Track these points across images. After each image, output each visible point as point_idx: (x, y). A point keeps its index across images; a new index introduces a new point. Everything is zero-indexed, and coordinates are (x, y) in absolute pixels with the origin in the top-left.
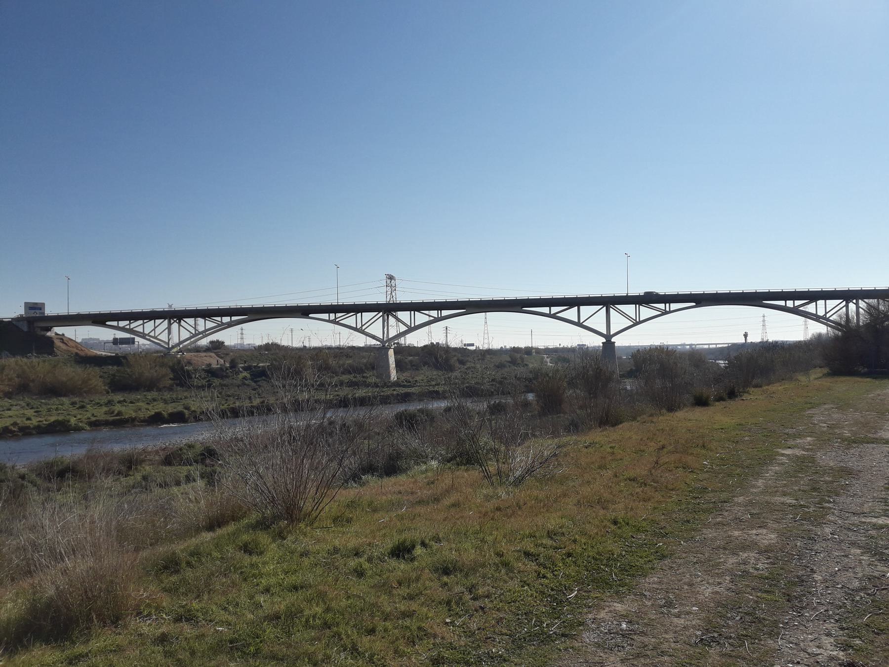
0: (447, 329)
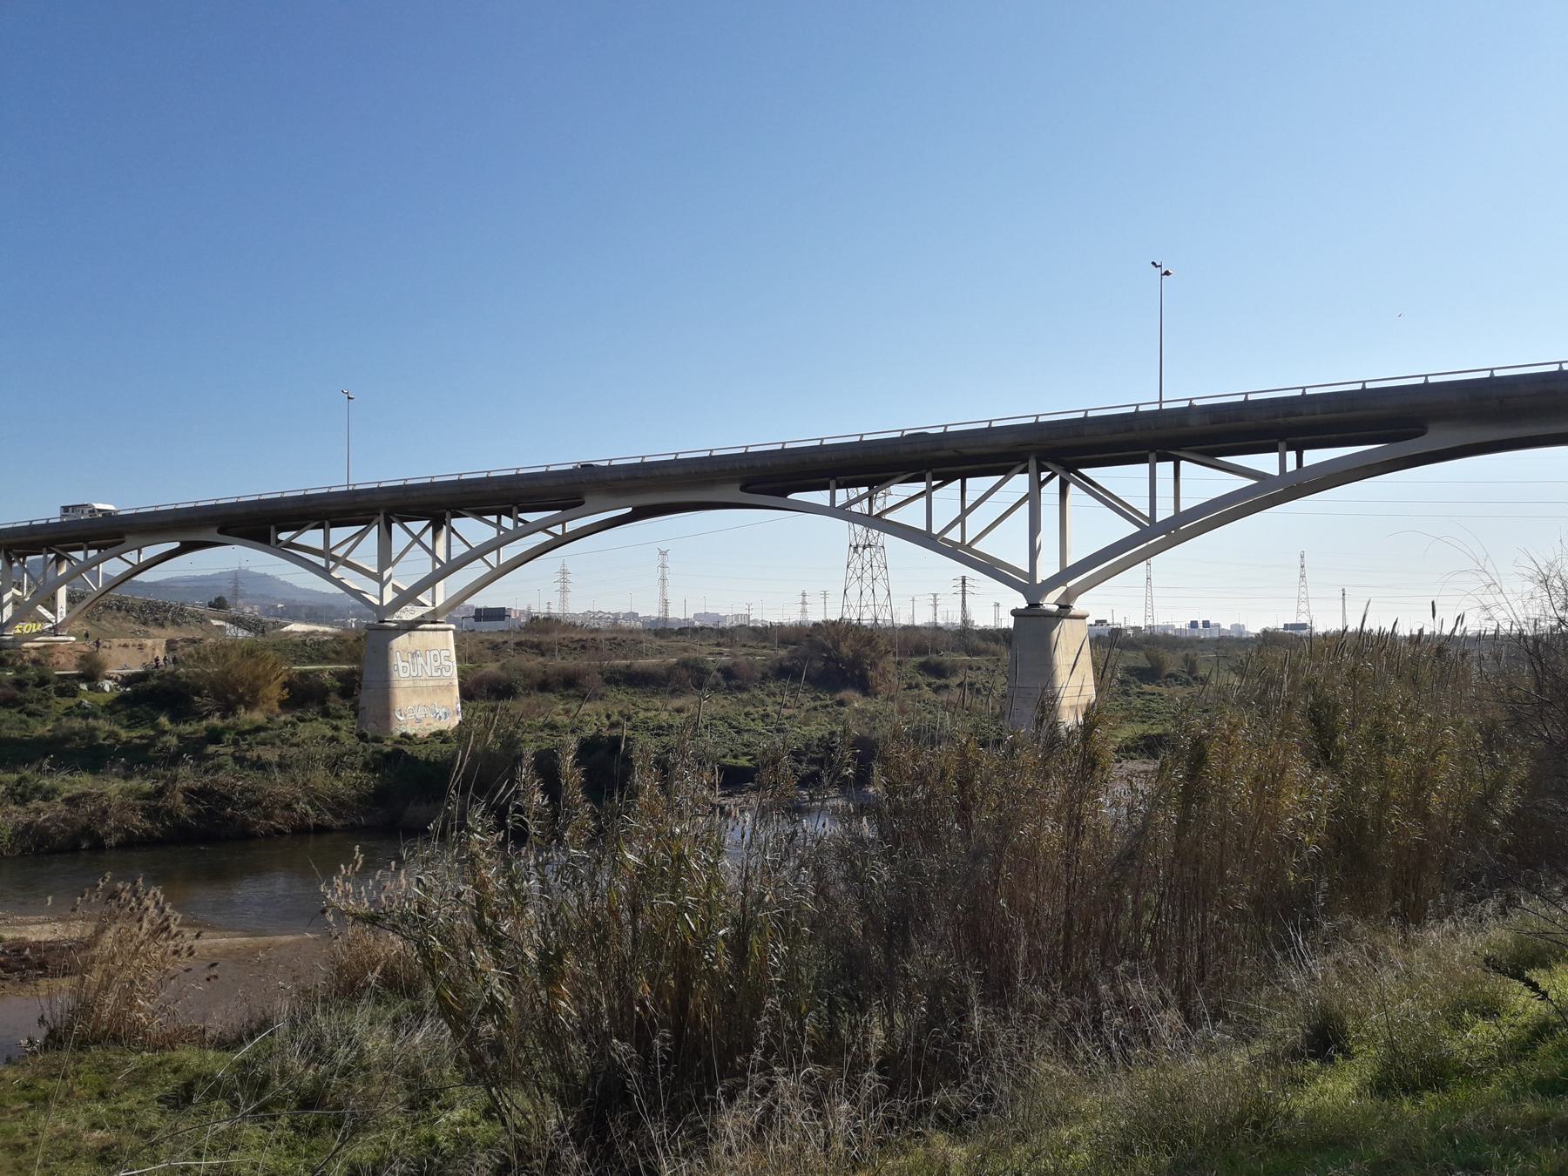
0: (964, 582)
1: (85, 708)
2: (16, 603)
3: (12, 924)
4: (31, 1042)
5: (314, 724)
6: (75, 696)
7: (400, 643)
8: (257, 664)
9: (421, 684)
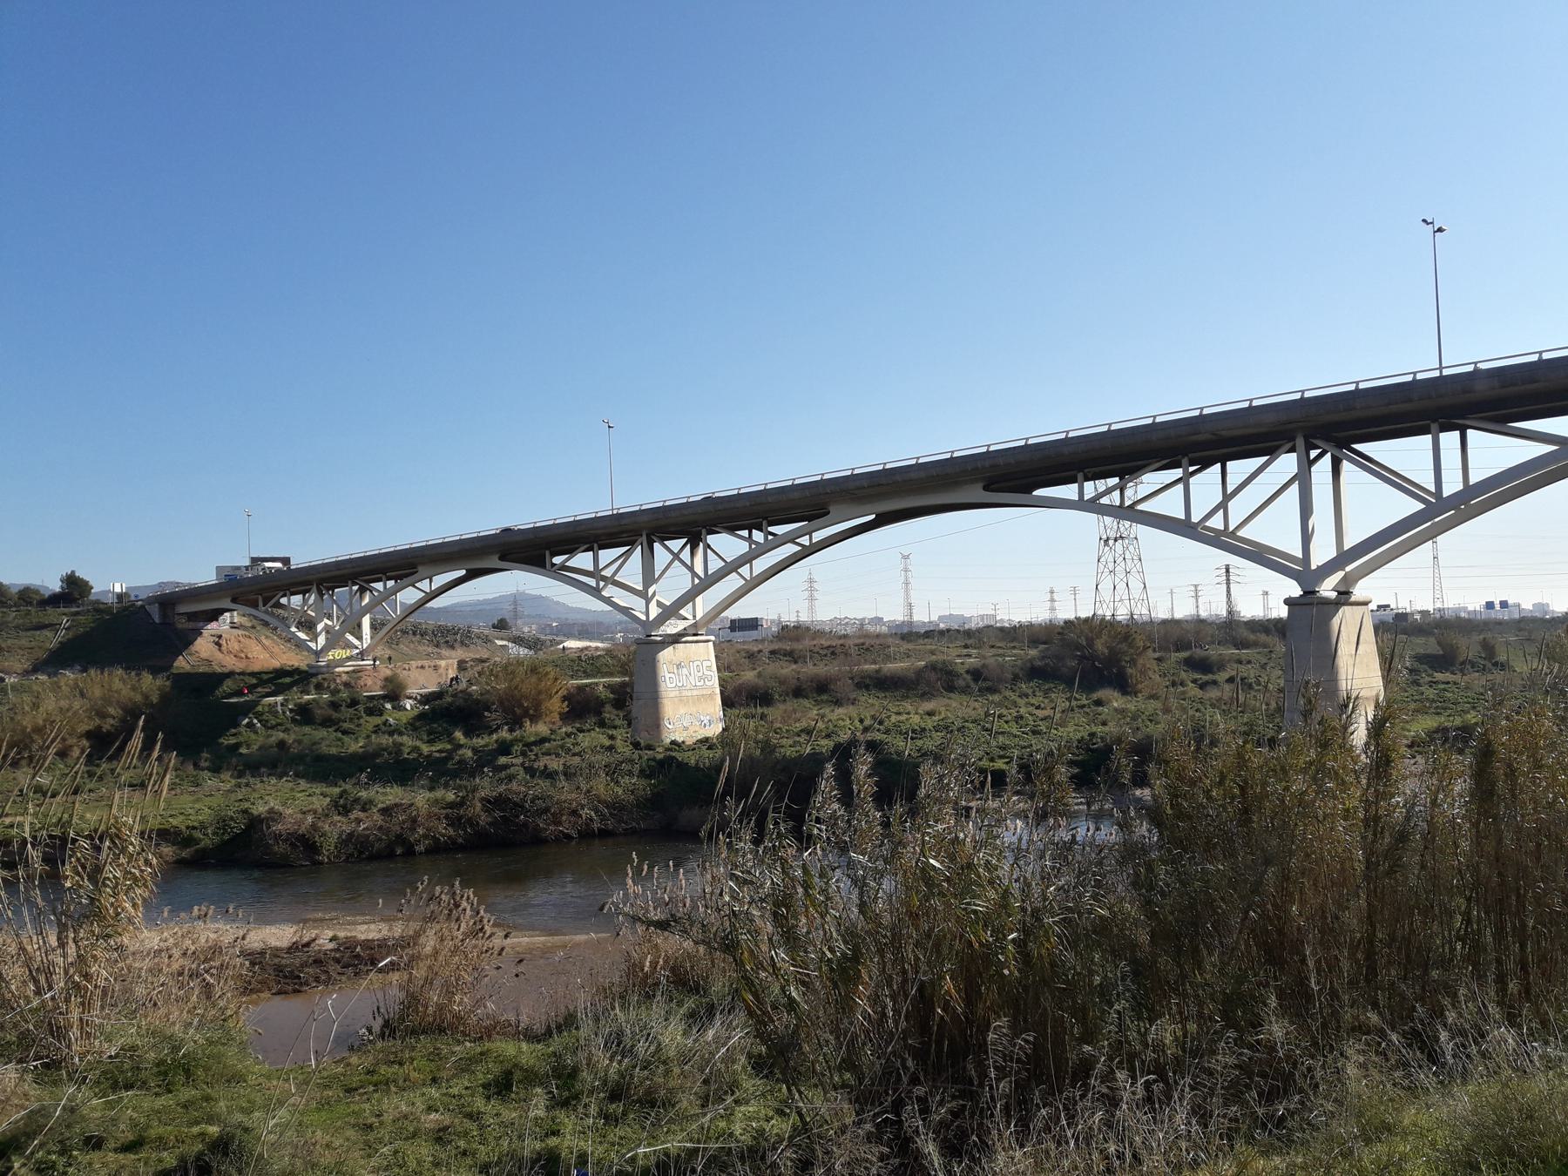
0: (1227, 571)
1: (390, 725)
2: (327, 632)
3: (343, 924)
4: (370, 1030)
5: (593, 734)
6: (381, 715)
7: (666, 656)
8: (540, 680)
9: (685, 693)
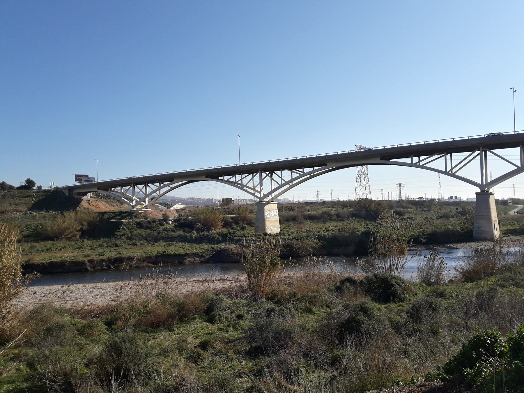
7: (266, 208)
